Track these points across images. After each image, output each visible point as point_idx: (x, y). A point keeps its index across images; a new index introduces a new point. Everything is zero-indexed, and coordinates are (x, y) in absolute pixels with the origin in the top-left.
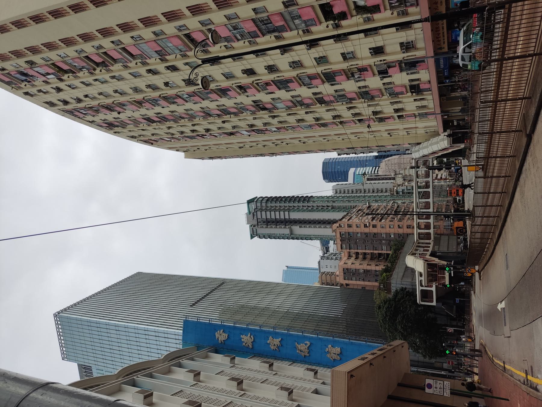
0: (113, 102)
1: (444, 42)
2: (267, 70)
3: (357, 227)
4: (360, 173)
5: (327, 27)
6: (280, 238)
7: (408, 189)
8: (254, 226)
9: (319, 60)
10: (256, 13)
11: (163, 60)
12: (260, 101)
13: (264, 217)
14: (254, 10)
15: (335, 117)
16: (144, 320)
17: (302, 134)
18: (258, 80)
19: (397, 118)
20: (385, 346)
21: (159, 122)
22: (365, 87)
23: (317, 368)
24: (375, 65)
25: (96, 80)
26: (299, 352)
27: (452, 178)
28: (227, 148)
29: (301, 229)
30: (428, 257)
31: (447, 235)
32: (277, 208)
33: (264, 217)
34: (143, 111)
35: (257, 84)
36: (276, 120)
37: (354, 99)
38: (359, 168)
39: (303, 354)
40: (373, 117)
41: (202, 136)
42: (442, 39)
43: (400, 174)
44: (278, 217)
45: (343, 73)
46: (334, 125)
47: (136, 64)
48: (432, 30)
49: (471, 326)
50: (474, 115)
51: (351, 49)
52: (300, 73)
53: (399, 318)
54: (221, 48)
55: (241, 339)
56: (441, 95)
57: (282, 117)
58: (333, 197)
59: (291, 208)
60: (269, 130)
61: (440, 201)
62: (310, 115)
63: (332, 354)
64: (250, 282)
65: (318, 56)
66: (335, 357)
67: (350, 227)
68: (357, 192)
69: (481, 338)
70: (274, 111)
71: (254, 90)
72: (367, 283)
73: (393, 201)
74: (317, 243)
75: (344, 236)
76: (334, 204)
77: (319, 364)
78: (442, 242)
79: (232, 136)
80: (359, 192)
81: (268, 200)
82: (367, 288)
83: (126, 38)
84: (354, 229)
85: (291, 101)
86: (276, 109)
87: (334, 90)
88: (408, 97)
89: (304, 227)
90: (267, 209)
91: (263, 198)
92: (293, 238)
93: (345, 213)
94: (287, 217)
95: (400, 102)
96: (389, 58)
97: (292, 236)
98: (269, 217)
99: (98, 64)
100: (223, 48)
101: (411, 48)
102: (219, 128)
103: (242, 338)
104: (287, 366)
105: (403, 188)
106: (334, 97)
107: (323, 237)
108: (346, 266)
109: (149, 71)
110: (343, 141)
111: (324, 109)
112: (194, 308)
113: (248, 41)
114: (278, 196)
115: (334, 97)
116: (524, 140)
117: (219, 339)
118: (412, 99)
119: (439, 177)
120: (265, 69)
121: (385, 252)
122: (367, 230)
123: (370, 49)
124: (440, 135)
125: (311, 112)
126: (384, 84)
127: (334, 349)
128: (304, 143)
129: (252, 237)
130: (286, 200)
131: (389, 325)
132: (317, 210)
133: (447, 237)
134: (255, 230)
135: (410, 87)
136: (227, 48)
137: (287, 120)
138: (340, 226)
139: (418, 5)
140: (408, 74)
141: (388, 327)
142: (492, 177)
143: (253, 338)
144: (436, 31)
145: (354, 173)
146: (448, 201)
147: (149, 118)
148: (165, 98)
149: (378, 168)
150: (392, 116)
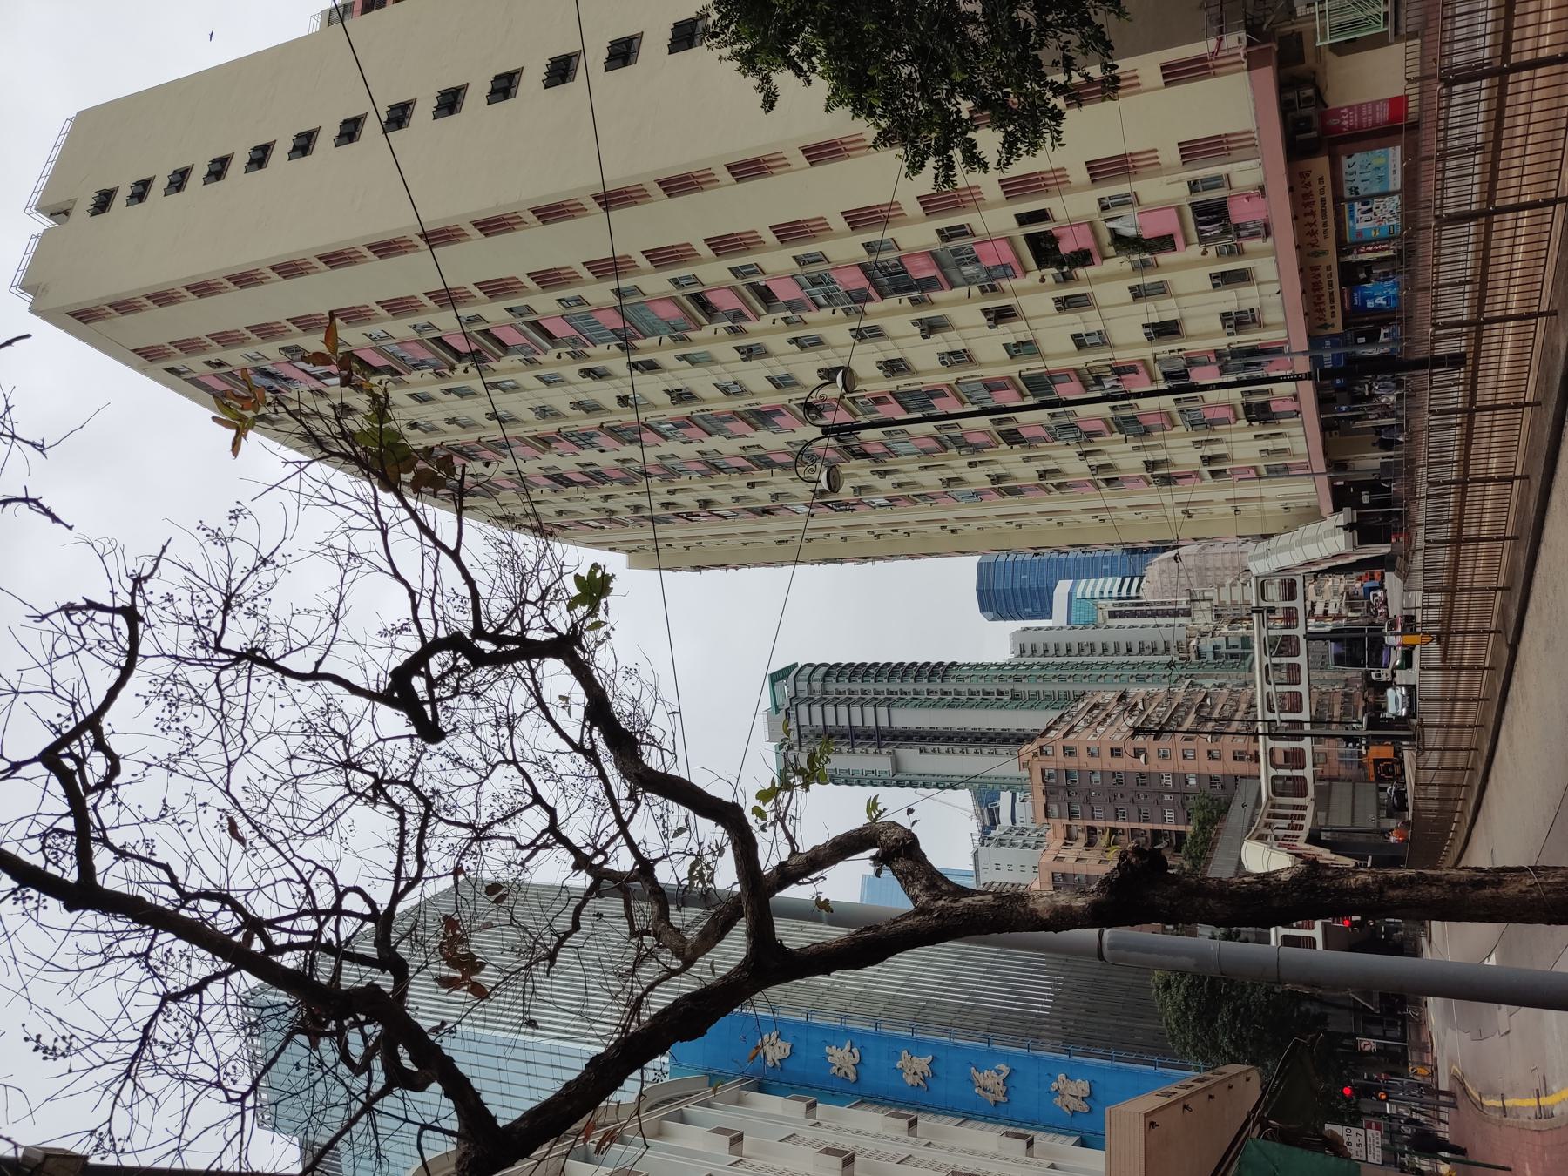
0: (479, 440)
3: (1092, 755)
4: (1088, 595)
5: (1043, 280)
10: (870, 252)
11: (626, 347)
13: (818, 721)
14: (867, 246)
15: (1043, 474)
17: (950, 512)
19: (1208, 476)
20: (1208, 1074)
21: (585, 484)
23: (1031, 1133)
24: (1155, 360)
25: (449, 391)
26: (981, 1092)
27: (1358, 614)
29: (925, 756)
30: (1302, 845)
31: (1349, 780)
32: (855, 697)
33: (818, 721)
34: (550, 459)
36: (890, 479)
38: (1084, 581)
39: (991, 1098)
41: (689, 516)
42: (1328, 306)
44: (857, 722)
45: (1073, 376)
47: (559, 356)
48: (1303, 292)
49: (1425, 1038)
50: (1414, 481)
53: (1223, 1016)
56: (1326, 427)
58: (1015, 667)
59: (895, 697)
60: (867, 504)
61: (1323, 682)
62: (979, 468)
63: (1068, 1097)
66: (1076, 1105)
67: (1071, 754)
68: (1081, 651)
69: (1452, 1061)
73: (1188, 681)
74: (964, 799)
75: (1053, 781)
76: (1019, 687)
77: (1036, 1124)
78: (1335, 800)
79: (766, 517)
80: (1087, 650)
81: (828, 674)
83: (545, 304)
84: (1081, 762)
88: (1241, 429)
89: (934, 751)
91: (816, 668)
92: (900, 784)
93: (1055, 714)
94: (884, 722)
96: (1191, 346)
98: (831, 721)
99: (459, 356)
100: (780, 323)
102: (737, 499)
104: (952, 1126)
106: (1048, 428)
107: (987, 780)
108: (1059, 867)
109: (587, 373)
114: (845, 662)
115: (1048, 428)
116: (1506, 652)
117: (769, 1057)
118: (1251, 435)
119: (1319, 611)
121: (1173, 828)
122: (1118, 764)
124: (1325, 519)
127: (1072, 1085)
128: (953, 531)
130: (880, 673)
131: (1195, 1036)
132: (971, 702)
133: (1348, 787)
136: (788, 323)
137: (916, 479)
138: (1042, 752)
139: (1268, 234)
141: (1193, 1040)
142: (1460, 669)
143: (857, 1055)
144: (1314, 291)
145: (1070, 595)
146: (1347, 683)
147: (561, 475)
148: (613, 431)
149: (1140, 582)
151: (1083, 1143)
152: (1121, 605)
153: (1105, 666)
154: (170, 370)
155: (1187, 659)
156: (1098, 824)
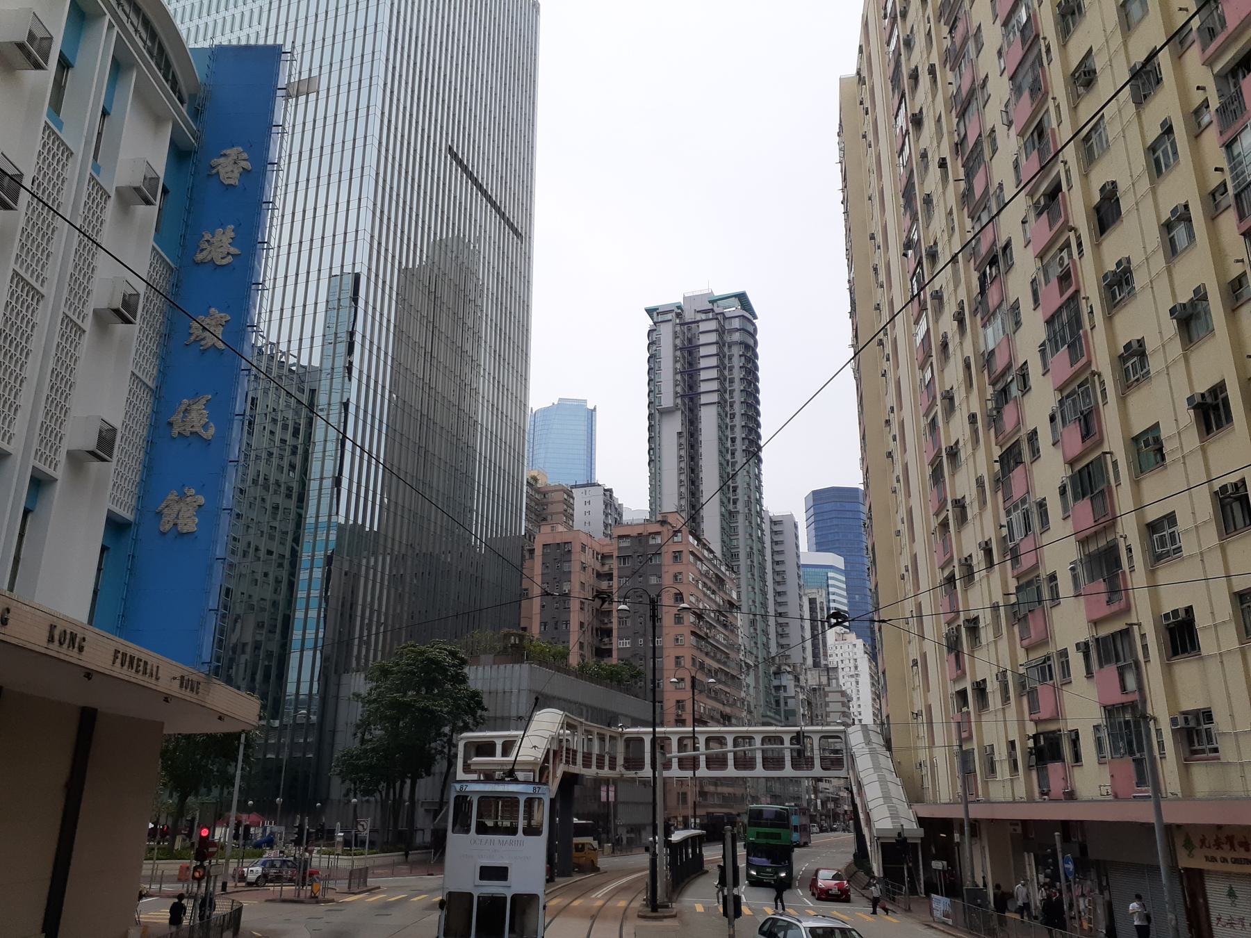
1: (1214, 860)
2: (1113, 268)
3: (675, 576)
6: (652, 383)
7: (789, 701)
8: (678, 315)
9: (1151, 441)
12: (1010, 267)
13: (703, 339)
15: (960, 505)
16: (447, 50)
18: (1080, 245)
19: (959, 687)
22: (1055, 597)
26: (183, 407)
28: (870, 199)
33: (703, 339)
35: (1067, 245)
37: (1015, 558)
38: (844, 579)
39: (177, 418)
40: (962, 617)
43: (829, 679)
46: (937, 505)
51: (1188, 545)
52: (1102, 383)
54: (1198, 88)
55: (222, 226)
57: (961, 343)
58: (759, 514)
64: (526, 306)
65: (1164, 434)
70: (979, 316)
71: (1047, 235)
72: (537, 602)
76: (741, 518)
80: (778, 579)
82: (524, 603)
85: (1008, 367)
86: (986, 319)
87: (1044, 499)
90: (724, 345)
91: (753, 335)
92: (651, 416)
95: (1006, 699)
97: (656, 414)
101: (1191, 743)
102: (924, 155)
103: (224, 229)
104: (131, 367)
105: (791, 691)
106: (1024, 501)
108: (576, 548)
110: (893, 535)
111: (983, 471)
112: (446, 157)
113: (1224, 184)
115: (1024, 501)
117: (222, 160)
120: (1120, 261)
121: (614, 647)
123: (1189, 610)
124: (910, 806)
125: (975, 432)
126: (1064, 653)
127: (192, 512)
128: (888, 422)
129: (650, 312)
134: (669, 316)
135: (1054, 732)
140: (1097, 728)
143: (224, 262)
145: (831, 567)
150: (964, 673)
151: (115, 526)
152: (822, 609)
153: (764, 593)
154: (984, 107)
155: (776, 667)
156: (615, 583)
